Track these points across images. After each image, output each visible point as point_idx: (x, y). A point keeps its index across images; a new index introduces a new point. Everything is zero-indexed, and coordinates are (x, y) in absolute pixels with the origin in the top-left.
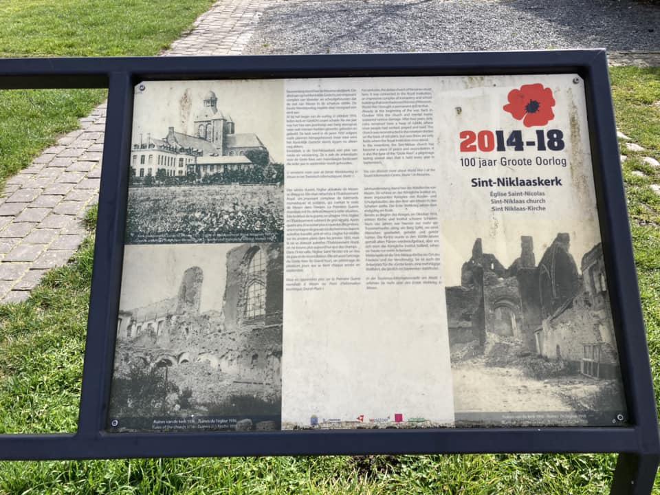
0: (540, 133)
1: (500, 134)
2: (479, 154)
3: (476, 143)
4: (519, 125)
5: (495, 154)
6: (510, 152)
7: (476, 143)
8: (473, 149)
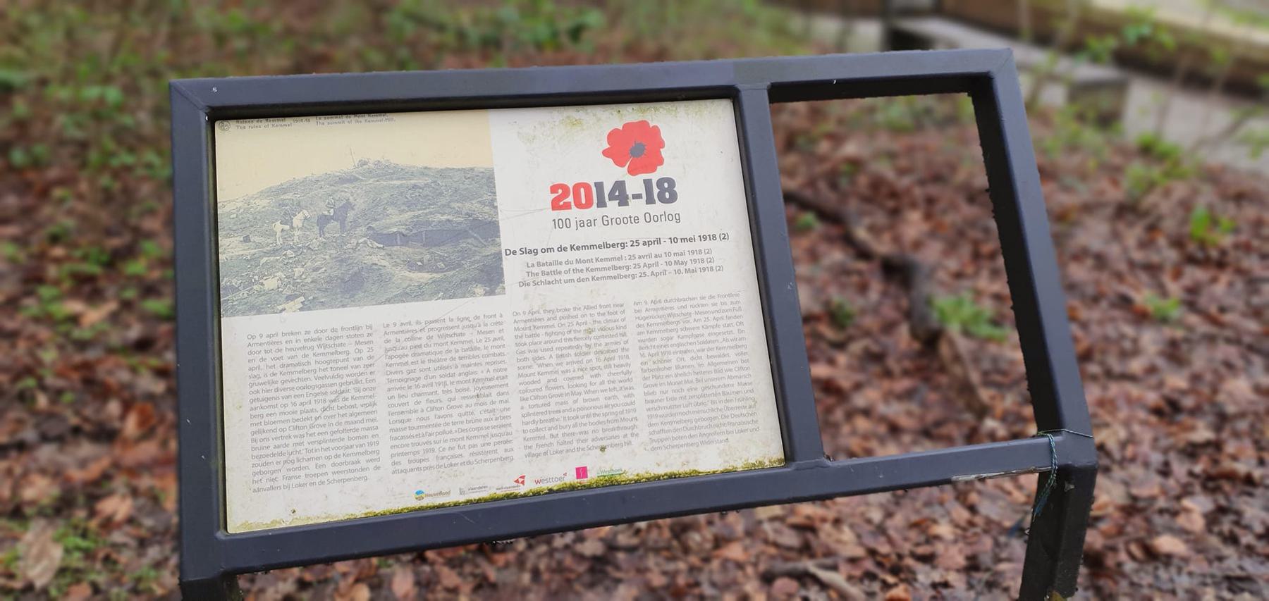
0: (648, 183)
1: (599, 186)
2: (574, 213)
3: (570, 199)
4: (621, 173)
5: (594, 212)
6: (613, 207)
7: (570, 199)
8: (567, 206)
